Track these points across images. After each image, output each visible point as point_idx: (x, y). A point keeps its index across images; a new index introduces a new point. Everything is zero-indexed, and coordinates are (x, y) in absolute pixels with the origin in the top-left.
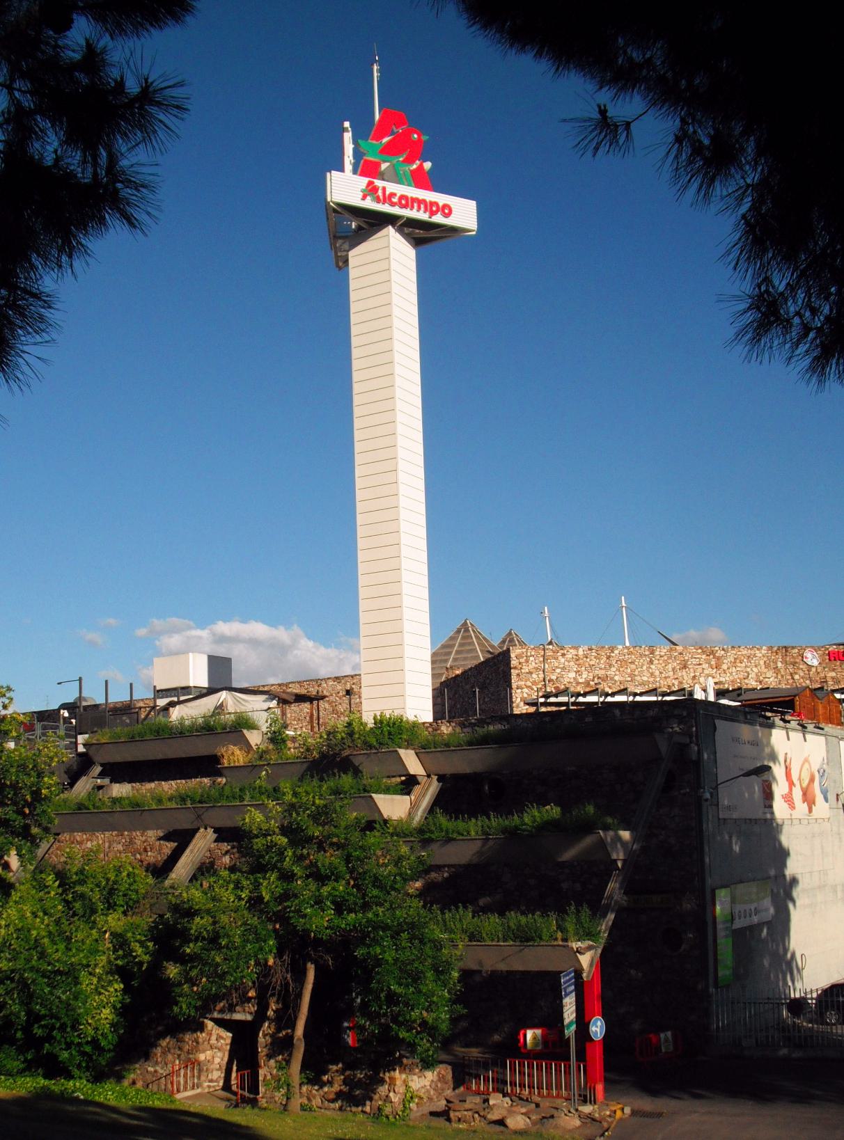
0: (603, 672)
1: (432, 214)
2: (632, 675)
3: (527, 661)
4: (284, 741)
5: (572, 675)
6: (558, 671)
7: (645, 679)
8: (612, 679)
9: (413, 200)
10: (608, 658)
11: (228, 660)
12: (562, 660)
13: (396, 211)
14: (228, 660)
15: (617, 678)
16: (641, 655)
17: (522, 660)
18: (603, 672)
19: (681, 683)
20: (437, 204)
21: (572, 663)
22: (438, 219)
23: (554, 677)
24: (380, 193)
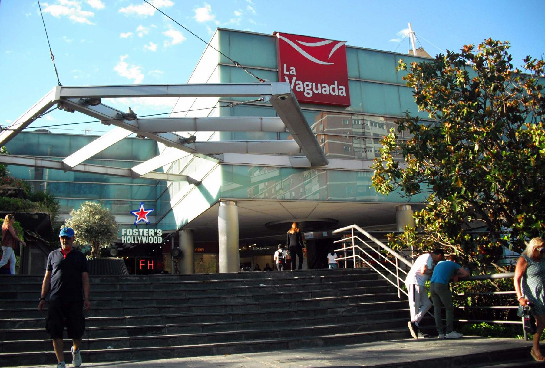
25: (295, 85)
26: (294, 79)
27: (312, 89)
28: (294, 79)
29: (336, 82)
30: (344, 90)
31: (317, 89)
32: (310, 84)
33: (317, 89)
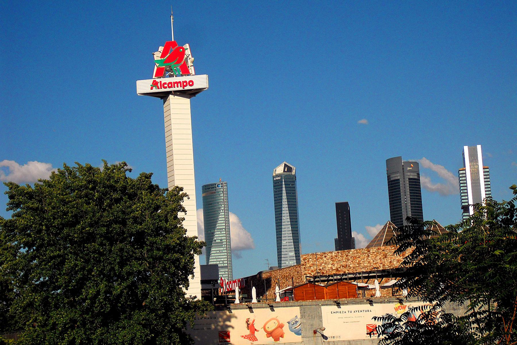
0: (345, 263)
1: (184, 86)
2: (359, 264)
3: (308, 261)
4: (461, 239)
5: (330, 266)
6: (323, 264)
7: (366, 265)
8: (349, 266)
9: (174, 83)
10: (347, 256)
11: (347, 203)
12: (325, 259)
13: (168, 90)
14: (347, 203)
15: (351, 266)
16: (363, 253)
17: (306, 261)
18: (345, 263)
19: (384, 265)
20: (186, 82)
21: (329, 260)
22: (188, 88)
23: (321, 268)
24: (159, 85)
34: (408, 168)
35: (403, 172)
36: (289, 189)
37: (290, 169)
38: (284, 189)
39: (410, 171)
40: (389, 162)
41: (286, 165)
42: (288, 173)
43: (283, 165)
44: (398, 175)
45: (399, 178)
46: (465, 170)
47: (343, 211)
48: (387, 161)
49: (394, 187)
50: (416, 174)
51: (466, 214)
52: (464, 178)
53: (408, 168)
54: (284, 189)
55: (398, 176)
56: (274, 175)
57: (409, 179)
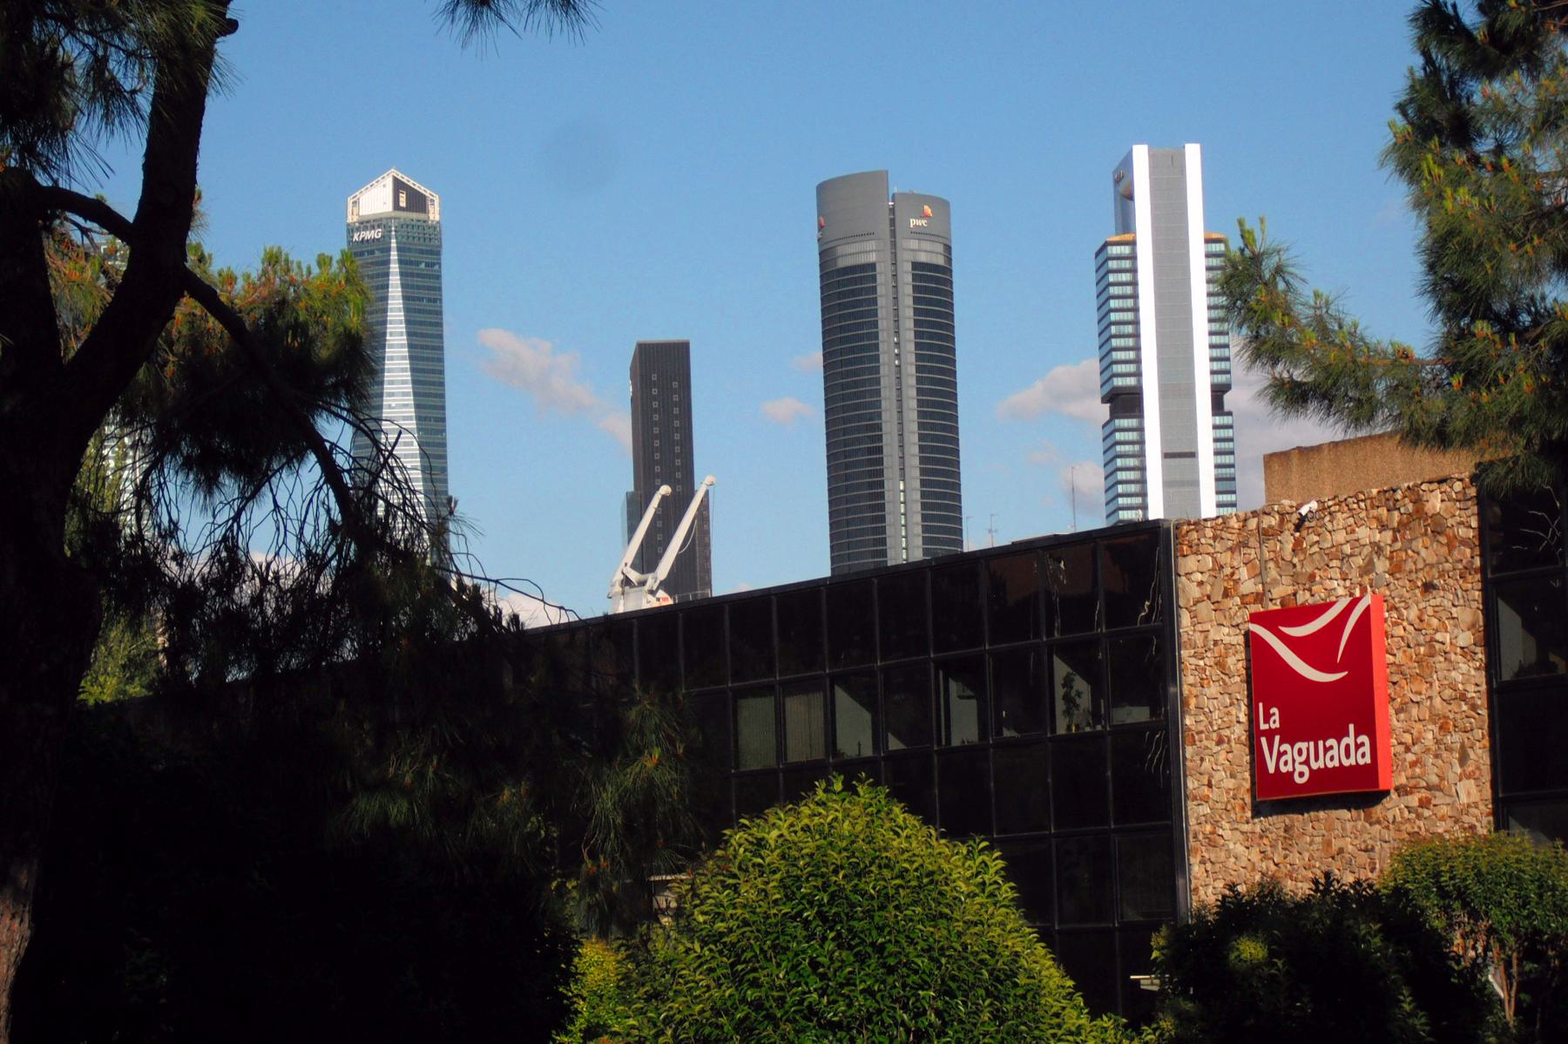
25: (1280, 755)
26: (1277, 738)
27: (1307, 762)
28: (1277, 738)
29: (1351, 727)
30: (1367, 749)
31: (1317, 759)
32: (1303, 745)
33: (1317, 759)
34: (913, 222)
35: (893, 234)
36: (418, 281)
37: (417, 202)
38: (394, 267)
39: (918, 233)
40: (826, 192)
41: (398, 186)
42: (415, 216)
43: (389, 182)
44: (872, 245)
45: (872, 258)
46: (1133, 243)
47: (662, 378)
48: (822, 189)
49: (846, 298)
50: (940, 248)
51: (1125, 423)
52: (1125, 277)
53: (913, 222)
54: (394, 267)
55: (868, 252)
56: (352, 219)
57: (916, 266)
